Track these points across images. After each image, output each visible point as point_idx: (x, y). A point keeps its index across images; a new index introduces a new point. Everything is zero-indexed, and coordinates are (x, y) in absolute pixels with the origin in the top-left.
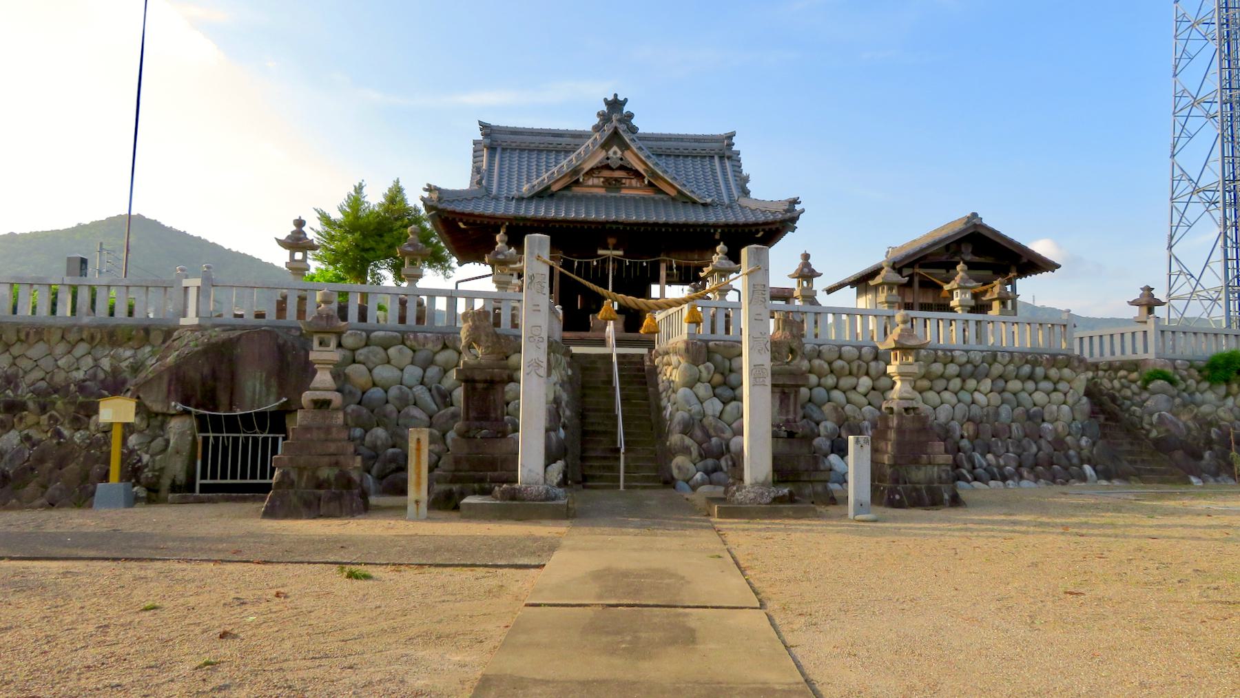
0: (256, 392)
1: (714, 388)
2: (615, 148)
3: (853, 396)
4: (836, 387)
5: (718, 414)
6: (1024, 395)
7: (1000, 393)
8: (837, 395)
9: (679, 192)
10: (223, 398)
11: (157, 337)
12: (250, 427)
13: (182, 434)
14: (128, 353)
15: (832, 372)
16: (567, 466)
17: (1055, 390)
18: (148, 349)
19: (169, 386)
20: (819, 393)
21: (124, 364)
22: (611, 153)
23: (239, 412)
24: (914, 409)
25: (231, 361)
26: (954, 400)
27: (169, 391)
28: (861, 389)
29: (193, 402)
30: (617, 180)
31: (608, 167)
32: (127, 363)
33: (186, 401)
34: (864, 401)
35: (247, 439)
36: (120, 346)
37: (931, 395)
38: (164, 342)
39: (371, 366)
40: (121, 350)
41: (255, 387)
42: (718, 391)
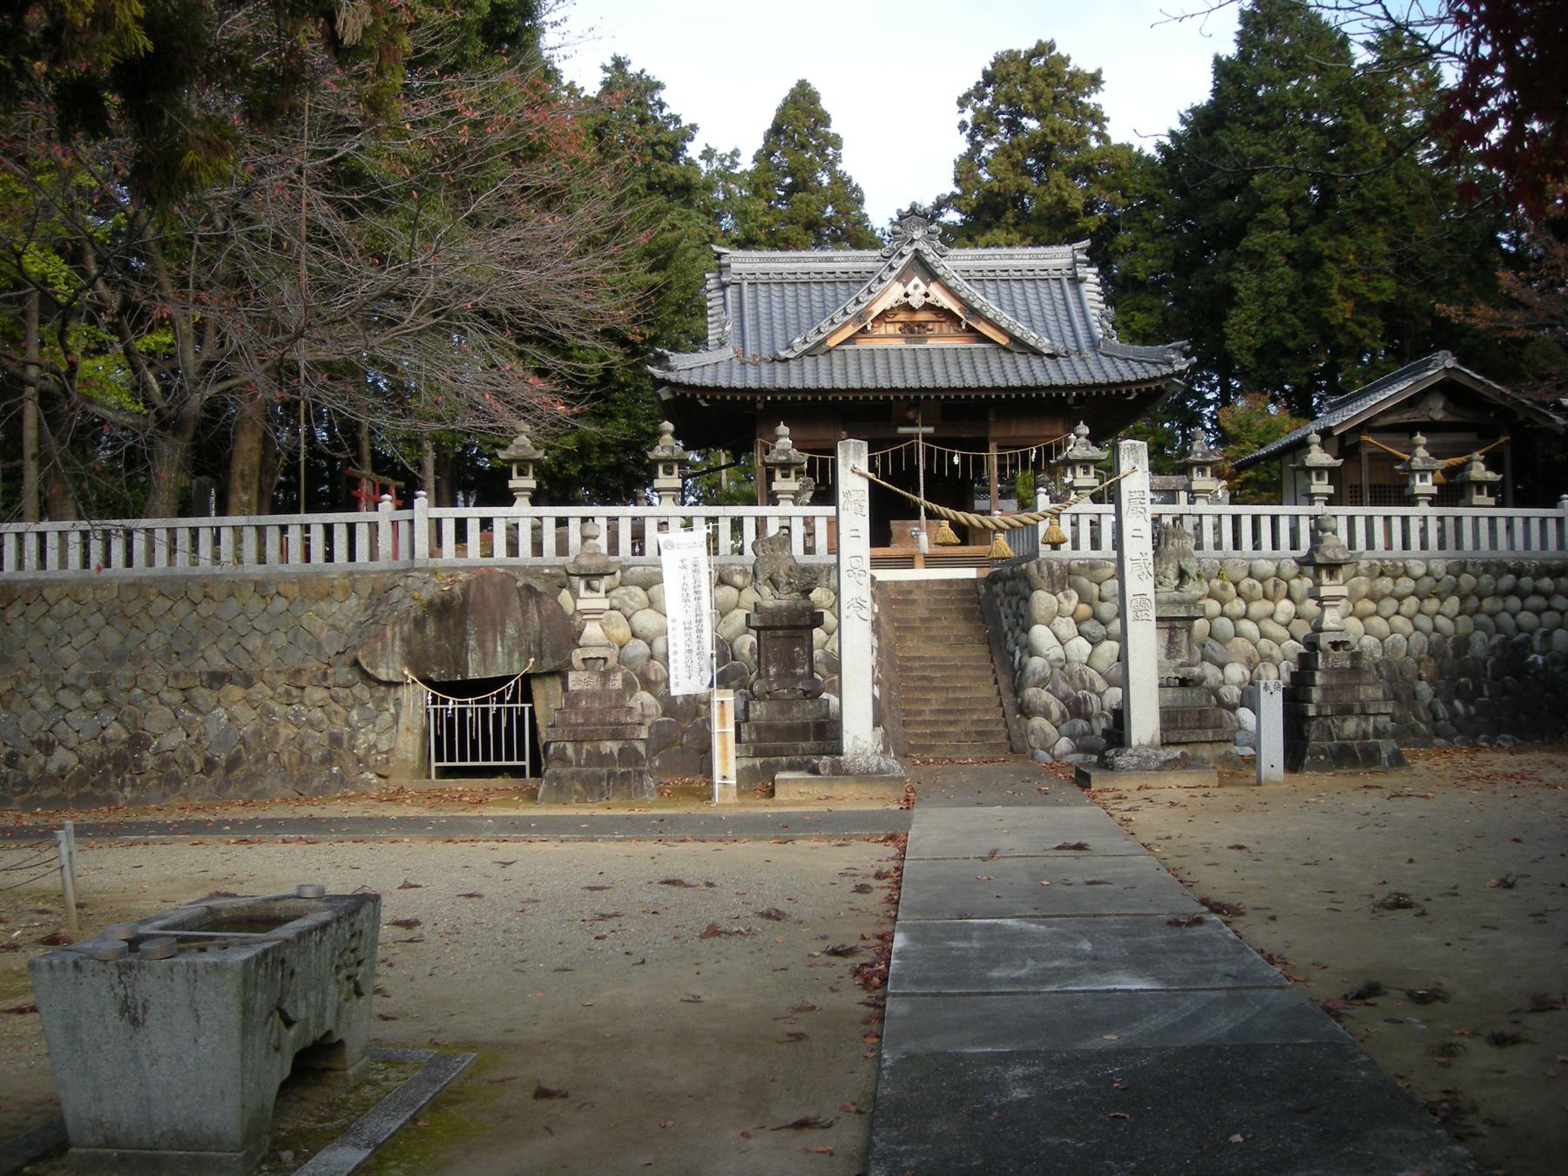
0: (493, 657)
1: (1078, 623)
2: (916, 280)
3: (1269, 626)
4: (1246, 616)
5: (1085, 659)
6: (1505, 617)
7: (1471, 615)
8: (1247, 626)
9: (1013, 338)
15: (1239, 595)
16: (886, 733)
17: (1549, 608)
20: (1225, 625)
22: (910, 288)
24: (1344, 643)
26: (1409, 628)
28: (1281, 617)
30: (921, 325)
31: (908, 308)
34: (1283, 632)
35: (499, 710)
37: (1376, 621)
39: (629, 612)
42: (1086, 627)
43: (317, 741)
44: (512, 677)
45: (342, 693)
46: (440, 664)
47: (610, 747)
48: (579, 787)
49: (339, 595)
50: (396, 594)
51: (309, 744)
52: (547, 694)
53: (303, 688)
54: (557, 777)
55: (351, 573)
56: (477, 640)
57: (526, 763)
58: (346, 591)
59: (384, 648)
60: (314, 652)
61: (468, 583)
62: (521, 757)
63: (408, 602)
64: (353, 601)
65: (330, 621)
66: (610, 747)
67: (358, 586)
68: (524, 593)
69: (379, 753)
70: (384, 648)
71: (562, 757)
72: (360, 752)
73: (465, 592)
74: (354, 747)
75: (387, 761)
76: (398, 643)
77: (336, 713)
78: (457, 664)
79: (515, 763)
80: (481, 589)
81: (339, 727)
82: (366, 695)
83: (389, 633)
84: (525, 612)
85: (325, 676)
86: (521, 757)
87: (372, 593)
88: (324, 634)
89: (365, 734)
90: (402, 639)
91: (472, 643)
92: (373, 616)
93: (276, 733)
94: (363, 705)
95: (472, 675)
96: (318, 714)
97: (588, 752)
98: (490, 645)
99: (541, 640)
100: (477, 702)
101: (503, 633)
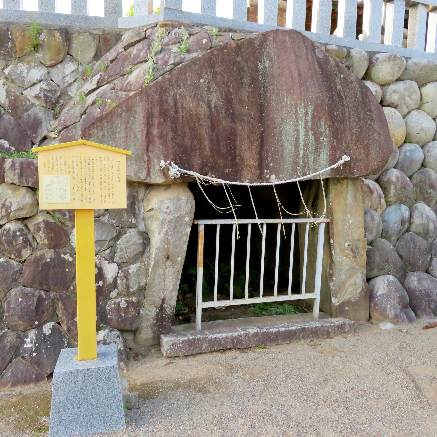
10: (249, 155)
11: (83, 48)
12: (269, 211)
13: (176, 223)
14: (37, 73)
18: (69, 67)
19: (149, 125)
21: (31, 93)
23: (274, 181)
25: (254, 81)
27: (149, 140)
29: (197, 161)
32: (36, 90)
33: (184, 163)
36: (20, 59)
38: (97, 56)
40: (22, 67)
41: (297, 131)
57: (316, 295)
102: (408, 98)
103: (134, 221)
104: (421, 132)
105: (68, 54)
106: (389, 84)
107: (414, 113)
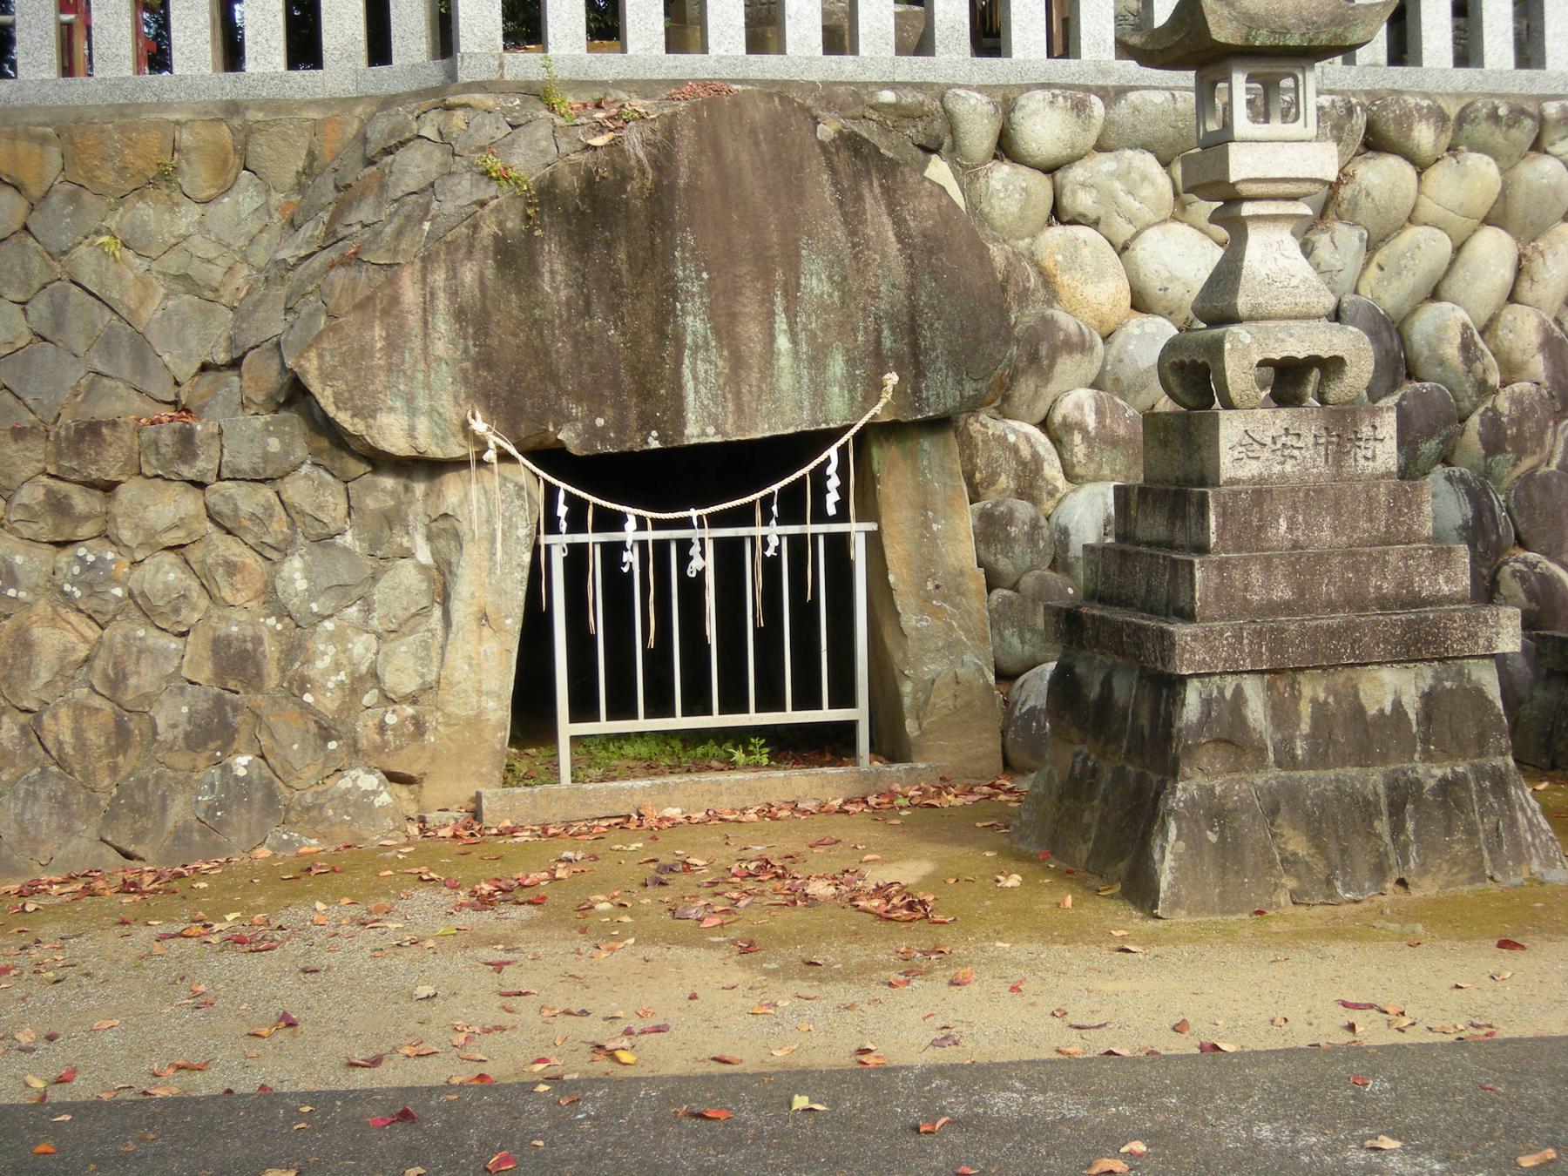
0: (762, 366)
35: (797, 545)
43: (169, 674)
44: (829, 437)
45: (248, 500)
46: (592, 396)
47: (1392, 687)
48: (1297, 844)
49: (197, 177)
50: (415, 166)
51: (143, 679)
52: (923, 489)
53: (108, 488)
54: (1216, 812)
55: (233, 108)
56: (712, 314)
57: (860, 713)
58: (221, 168)
59: (394, 344)
60: (126, 365)
61: (670, 126)
62: (843, 696)
63: (464, 190)
64: (246, 199)
65: (173, 263)
66: (1392, 687)
67: (261, 148)
68: (842, 159)
69: (387, 699)
70: (394, 344)
71: (1232, 736)
72: (326, 700)
73: (663, 157)
74: (303, 684)
75: (419, 726)
76: (442, 325)
77: (232, 568)
78: (645, 394)
79: (826, 714)
80: (711, 145)
81: (243, 618)
82: (333, 504)
83: (410, 294)
84: (853, 221)
85: (187, 444)
86: (843, 696)
87: (309, 171)
88: (154, 309)
89: (337, 638)
90: (460, 314)
91: (694, 324)
92: (331, 238)
93: (23, 644)
94: (324, 540)
95: (696, 432)
96: (165, 574)
97: (1318, 707)
98: (751, 330)
99: (913, 312)
100: (716, 521)
101: (792, 291)
102: (1130, 198)
103: (406, 544)
104: (1171, 286)
105: (245, 168)
106: (1070, 161)
107: (1152, 234)
